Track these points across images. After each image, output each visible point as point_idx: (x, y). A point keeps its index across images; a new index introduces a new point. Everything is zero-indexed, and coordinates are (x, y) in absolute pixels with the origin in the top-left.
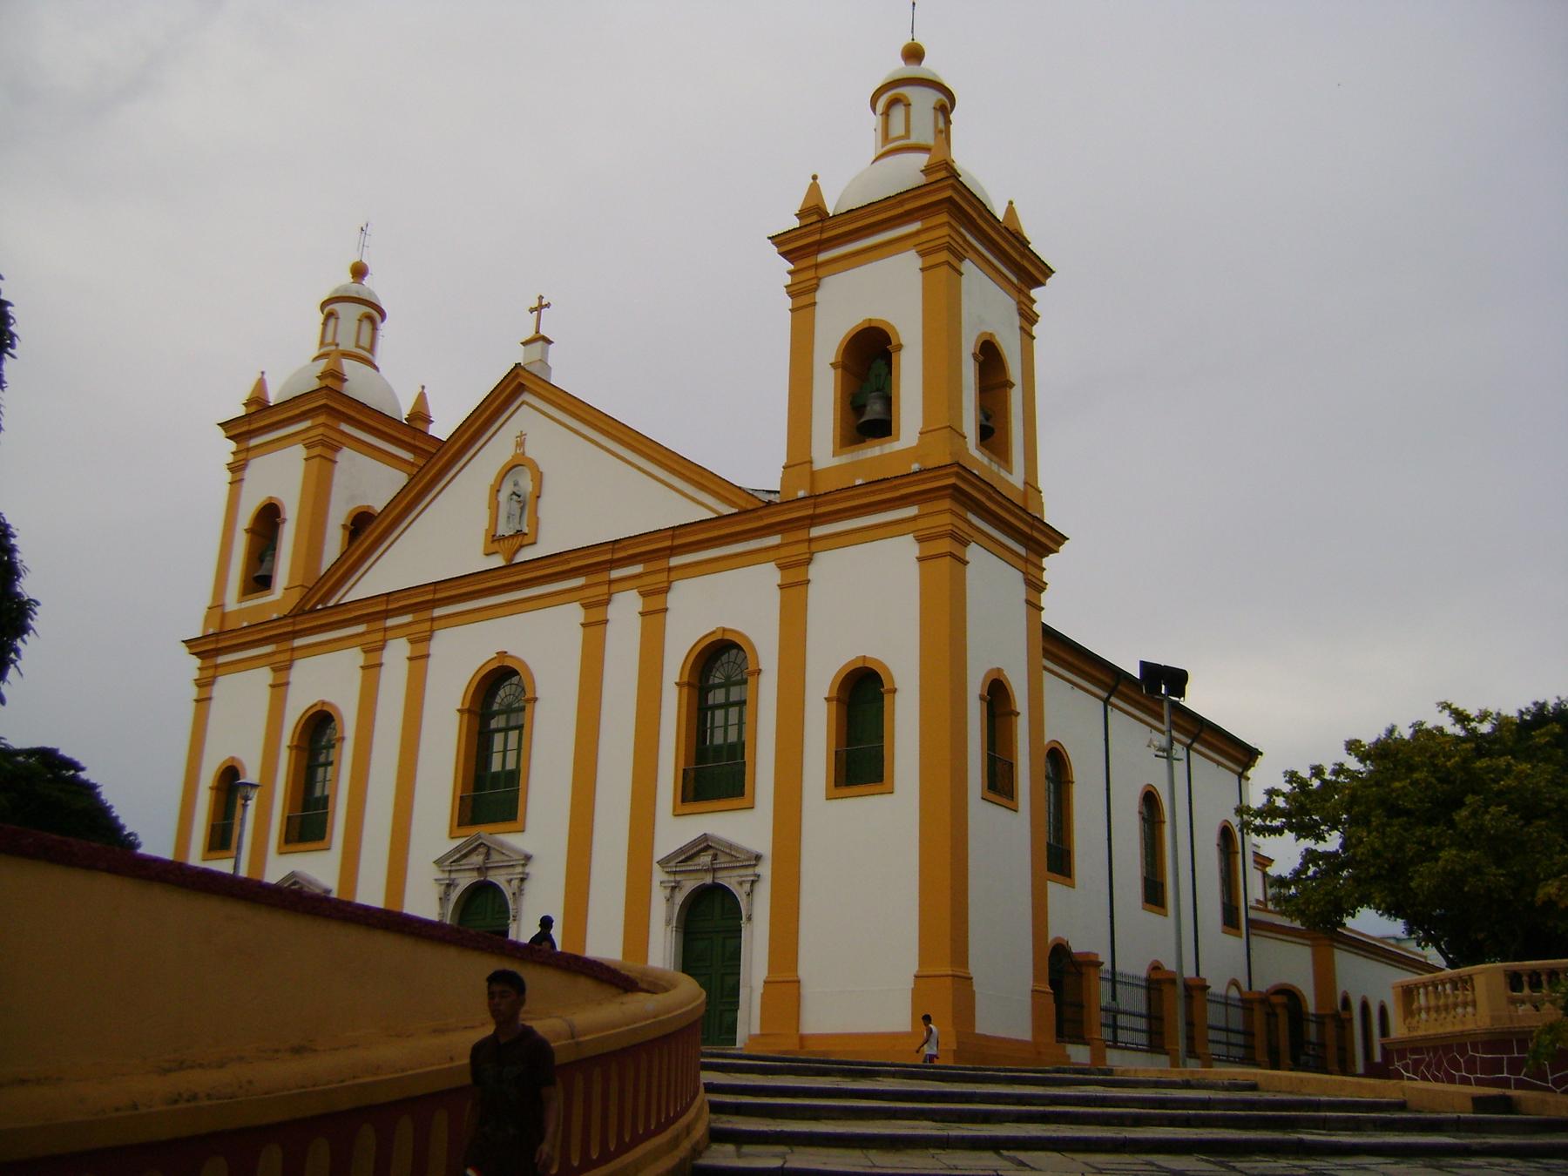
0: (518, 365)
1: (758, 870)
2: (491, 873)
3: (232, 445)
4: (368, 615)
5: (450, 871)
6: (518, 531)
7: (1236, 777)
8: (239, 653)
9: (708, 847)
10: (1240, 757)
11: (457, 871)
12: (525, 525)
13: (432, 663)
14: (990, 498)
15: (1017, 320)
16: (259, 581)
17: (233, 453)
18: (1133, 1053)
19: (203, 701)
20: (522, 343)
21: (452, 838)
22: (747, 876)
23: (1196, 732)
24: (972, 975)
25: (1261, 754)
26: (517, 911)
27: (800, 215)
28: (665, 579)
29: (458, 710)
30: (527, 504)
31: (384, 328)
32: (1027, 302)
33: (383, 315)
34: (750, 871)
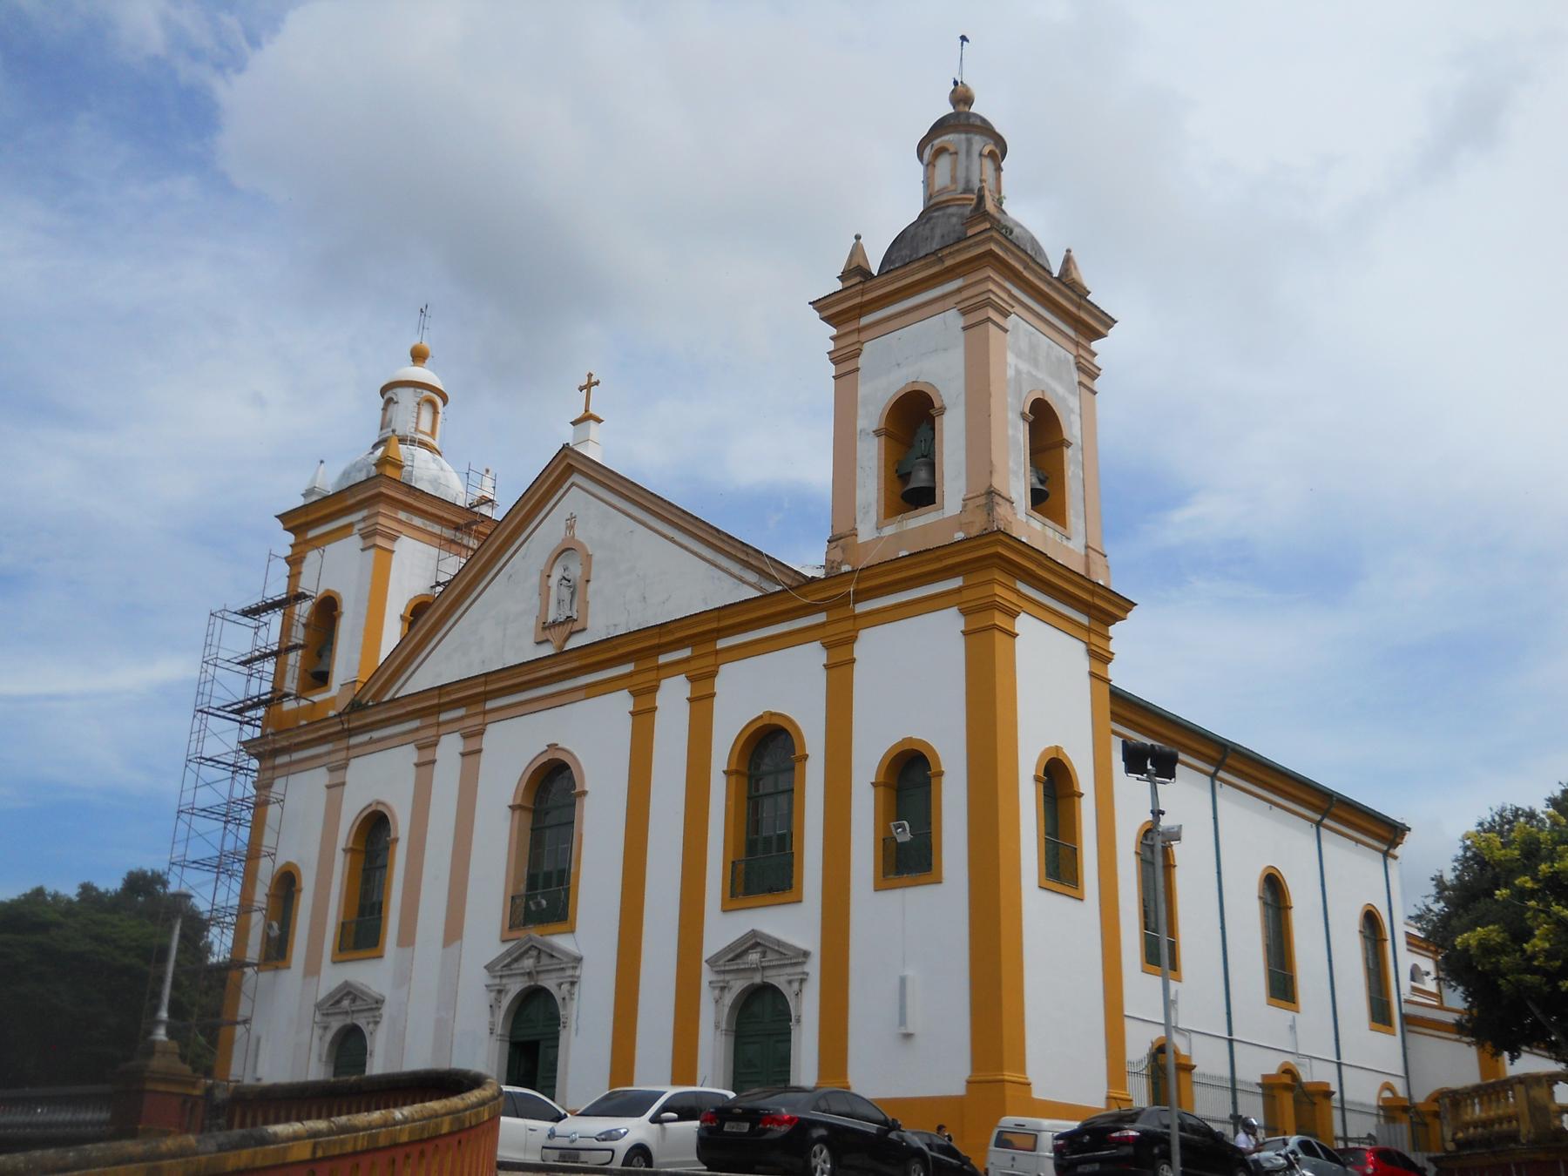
0: (566, 447)
1: (806, 968)
2: (542, 976)
3: (290, 538)
4: (965, 563)
5: (501, 977)
6: (568, 617)
7: (1380, 856)
8: (609, 670)
9: (757, 944)
10: (1386, 834)
11: (509, 976)
12: (575, 611)
13: (485, 758)
14: (1040, 565)
21: (504, 941)
22: (794, 974)
23: (1326, 806)
24: (1030, 1080)
25: (1409, 829)
30: (575, 589)
32: (1088, 357)
34: (798, 969)
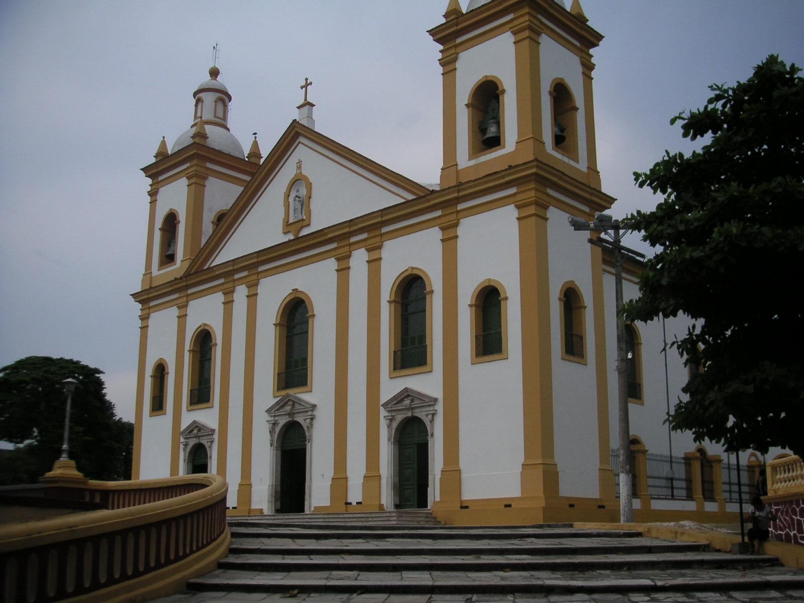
0: (294, 121)
1: (214, 437)
5: (275, 416)
14: (560, 178)
15: (580, 69)
16: (168, 258)
17: (150, 185)
18: (665, 501)
19: (144, 328)
20: (297, 107)
22: (429, 411)
24: (556, 463)
26: (311, 436)
27: (445, 16)
28: (380, 240)
29: (274, 324)
30: (305, 203)
31: (231, 105)
33: (230, 98)
34: (432, 408)
